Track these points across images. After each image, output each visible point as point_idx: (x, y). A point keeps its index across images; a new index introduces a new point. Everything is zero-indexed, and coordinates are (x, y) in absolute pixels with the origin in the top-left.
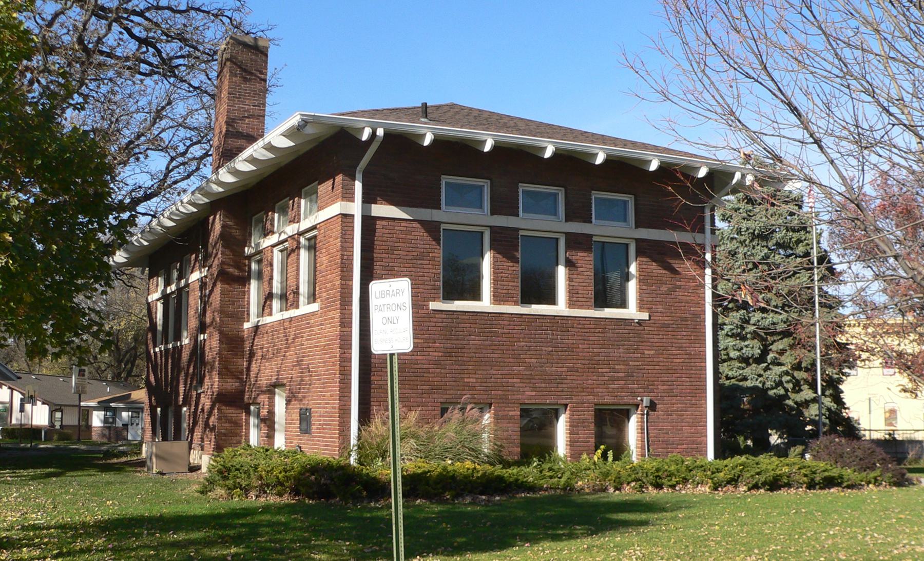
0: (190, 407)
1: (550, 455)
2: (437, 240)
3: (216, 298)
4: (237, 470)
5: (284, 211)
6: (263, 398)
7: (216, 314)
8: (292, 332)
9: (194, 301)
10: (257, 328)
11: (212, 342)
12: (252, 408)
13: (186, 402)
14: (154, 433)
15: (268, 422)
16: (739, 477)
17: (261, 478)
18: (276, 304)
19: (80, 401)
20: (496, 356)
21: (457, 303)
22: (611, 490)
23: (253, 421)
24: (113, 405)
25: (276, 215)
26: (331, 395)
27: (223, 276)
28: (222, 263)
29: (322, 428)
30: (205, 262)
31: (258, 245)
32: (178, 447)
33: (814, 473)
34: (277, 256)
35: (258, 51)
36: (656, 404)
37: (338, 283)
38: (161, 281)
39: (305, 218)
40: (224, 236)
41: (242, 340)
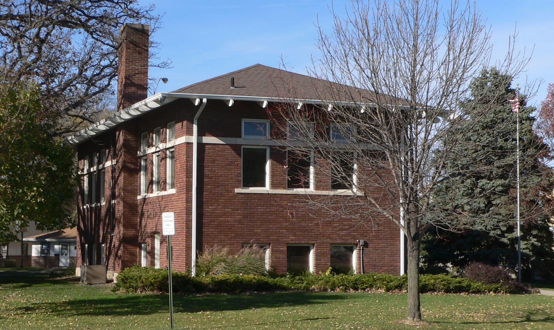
0: (107, 244)
1: (305, 272)
2: (239, 155)
3: (121, 180)
4: (131, 278)
5: (158, 133)
6: (148, 240)
7: (121, 190)
8: (163, 204)
9: (108, 177)
10: (144, 199)
11: (120, 209)
12: (143, 245)
13: (104, 241)
14: (83, 261)
15: (151, 254)
16: (402, 285)
17: (142, 282)
18: (155, 187)
19: (22, 238)
20: (273, 217)
21: (251, 189)
22: (329, 290)
23: (143, 253)
24: (47, 240)
25: (154, 135)
26: (182, 239)
27: (125, 168)
28: (124, 162)
29: (177, 257)
30: (115, 156)
31: (145, 151)
32: (99, 269)
33: (450, 284)
34: (155, 159)
35: (144, 32)
36: (368, 244)
37: (185, 179)
38: (86, 162)
39: (170, 141)
40: (126, 144)
41: (136, 206)
